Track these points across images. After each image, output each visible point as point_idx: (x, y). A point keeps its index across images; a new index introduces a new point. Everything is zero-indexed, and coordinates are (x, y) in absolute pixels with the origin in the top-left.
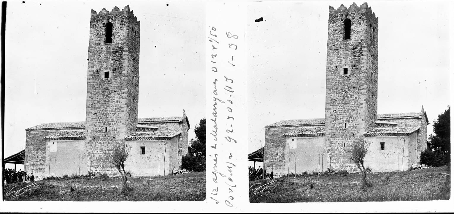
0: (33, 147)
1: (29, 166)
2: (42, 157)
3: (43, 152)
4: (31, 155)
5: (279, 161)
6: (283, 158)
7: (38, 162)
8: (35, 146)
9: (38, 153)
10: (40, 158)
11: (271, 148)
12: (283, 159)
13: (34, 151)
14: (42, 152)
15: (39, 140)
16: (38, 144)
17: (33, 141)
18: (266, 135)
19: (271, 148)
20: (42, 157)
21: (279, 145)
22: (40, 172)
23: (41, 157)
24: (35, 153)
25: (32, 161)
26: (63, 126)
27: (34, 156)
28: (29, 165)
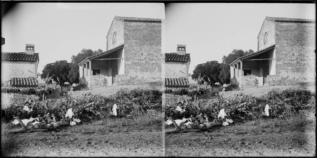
0: (286, 42)
1: (282, 65)
2: (147, 55)
3: (149, 49)
4: (132, 52)
5: (145, 62)
6: (302, 59)
7: (143, 60)
8: (288, 41)
9: (294, 50)
10: (146, 55)
11: (285, 46)
12: (301, 61)
13: (287, 48)
14: (299, 49)
15: (143, 34)
16: (141, 38)
17: (134, 34)
18: (126, 30)
19: (285, 46)
20: (299, 55)
21: (295, 44)
22: (298, 73)
23: (146, 54)
24: (290, 50)
25: (286, 59)
26: (142, 20)
27: (289, 53)
28: (282, 64)
